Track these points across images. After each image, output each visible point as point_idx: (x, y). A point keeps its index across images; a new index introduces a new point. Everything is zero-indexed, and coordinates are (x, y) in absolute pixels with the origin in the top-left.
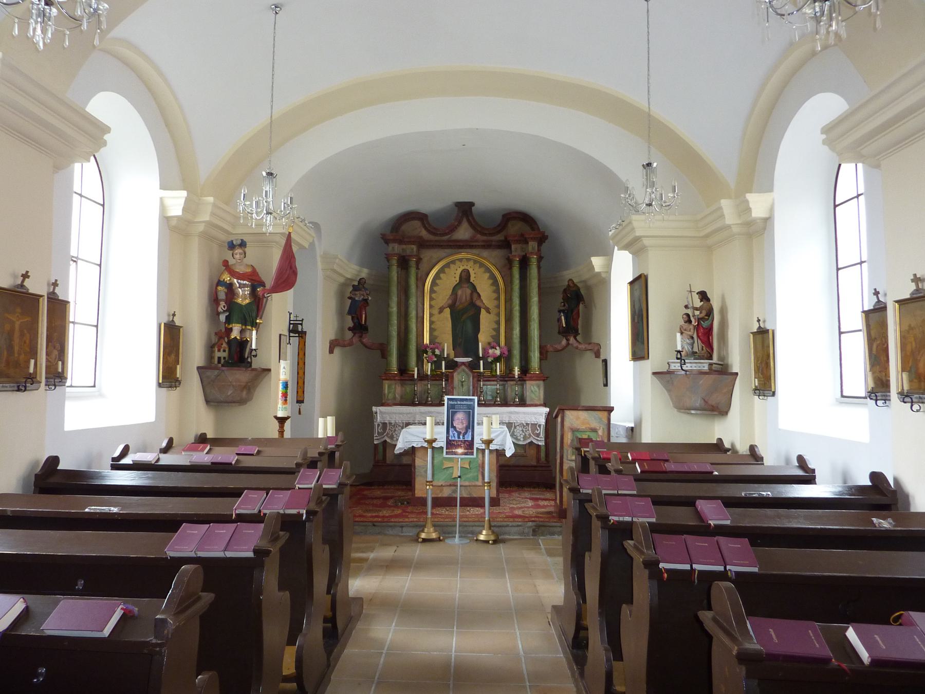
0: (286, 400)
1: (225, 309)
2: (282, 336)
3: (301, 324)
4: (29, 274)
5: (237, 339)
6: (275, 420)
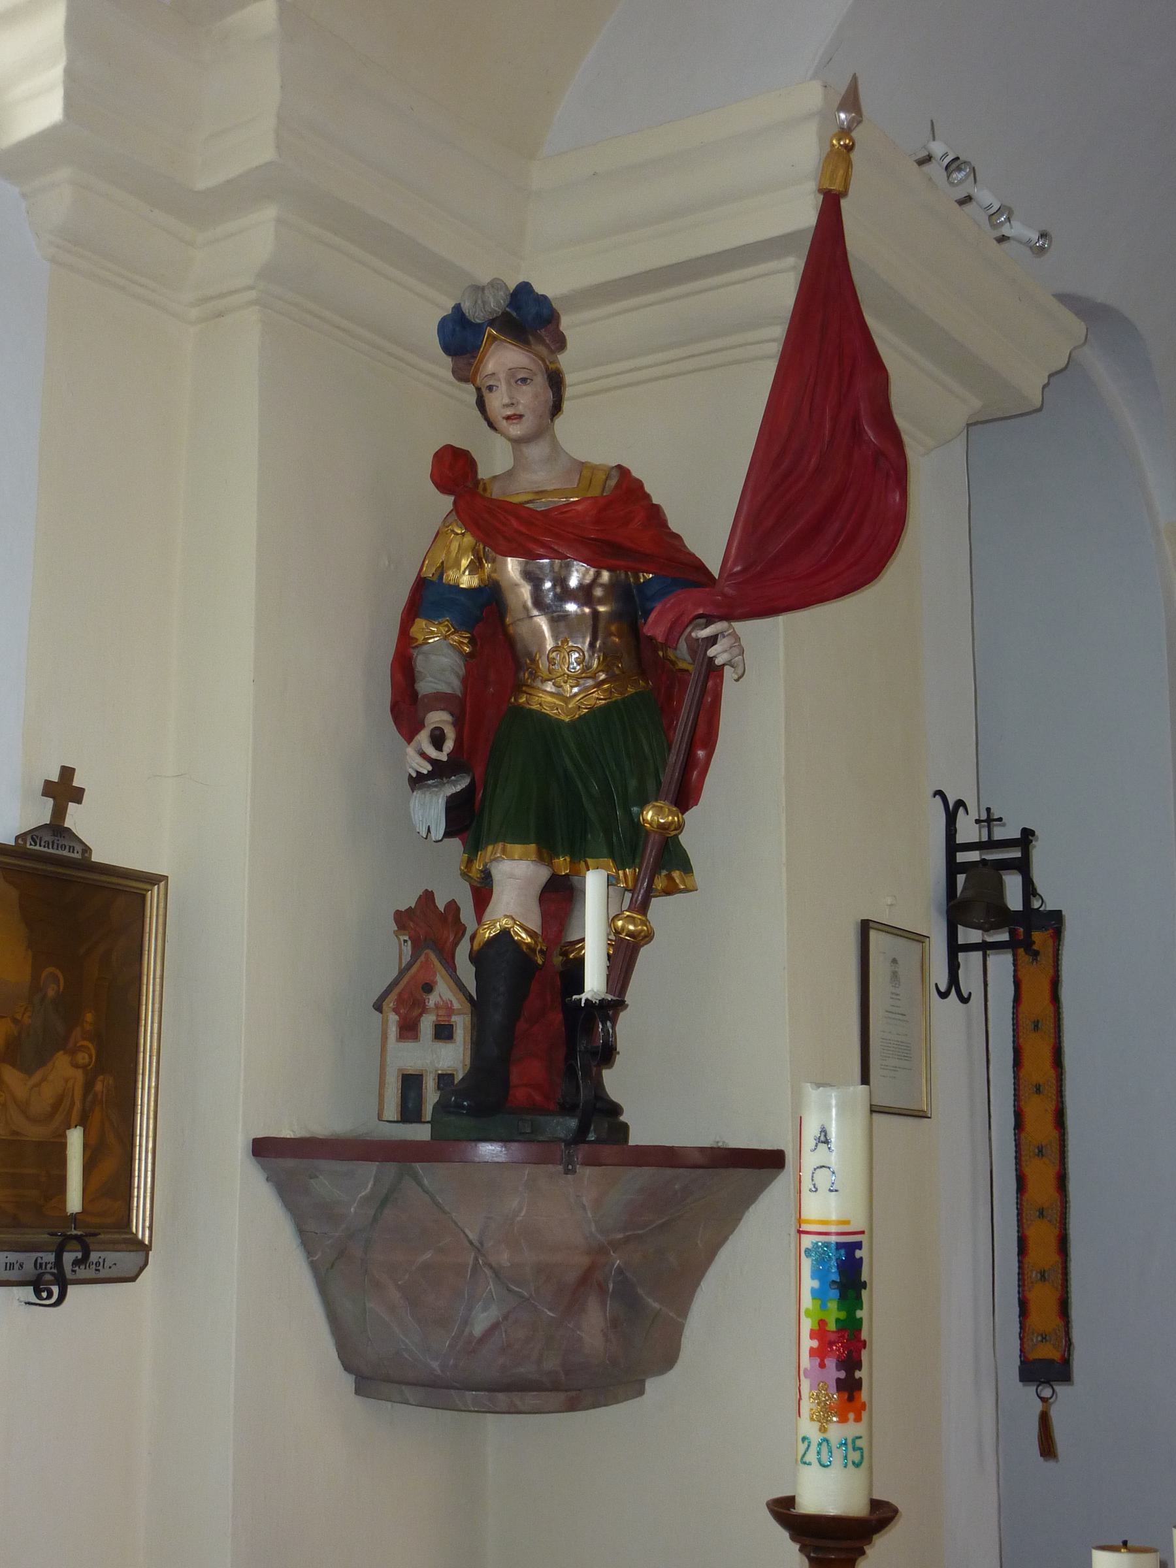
0: (849, 1388)
1: (443, 757)
2: (873, 935)
3: (1023, 866)
4: (76, 783)
5: (517, 945)
6: (782, 1535)
